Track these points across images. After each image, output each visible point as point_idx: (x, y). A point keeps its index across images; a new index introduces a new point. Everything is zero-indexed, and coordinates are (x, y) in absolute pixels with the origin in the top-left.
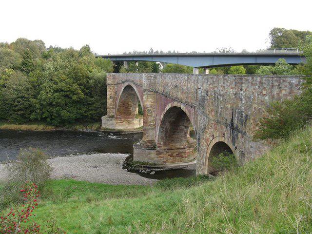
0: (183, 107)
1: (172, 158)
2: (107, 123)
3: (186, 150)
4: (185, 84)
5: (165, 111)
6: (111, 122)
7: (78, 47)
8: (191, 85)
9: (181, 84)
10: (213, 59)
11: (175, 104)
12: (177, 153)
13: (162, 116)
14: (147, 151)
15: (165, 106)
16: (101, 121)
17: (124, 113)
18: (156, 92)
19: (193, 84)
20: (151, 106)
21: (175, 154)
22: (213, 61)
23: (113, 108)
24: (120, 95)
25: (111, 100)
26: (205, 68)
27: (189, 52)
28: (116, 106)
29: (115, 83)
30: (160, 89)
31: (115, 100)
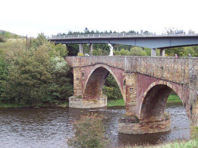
0: (169, 84)
1: (152, 130)
2: (74, 103)
3: (164, 122)
4: (171, 65)
5: (149, 88)
6: (78, 102)
7: (35, 36)
8: (178, 66)
9: (167, 65)
10: (171, 41)
11: (161, 82)
12: (157, 125)
13: (145, 93)
14: (131, 124)
15: (149, 85)
16: (68, 101)
17: (91, 93)
18: (137, 73)
19: (180, 65)
20: (133, 85)
21: (154, 126)
22: (171, 43)
23: (79, 89)
24: (88, 78)
25: (78, 81)
26: (162, 49)
27: (119, 31)
28: (83, 87)
29: (83, 65)
30: (143, 71)
31: (81, 81)
